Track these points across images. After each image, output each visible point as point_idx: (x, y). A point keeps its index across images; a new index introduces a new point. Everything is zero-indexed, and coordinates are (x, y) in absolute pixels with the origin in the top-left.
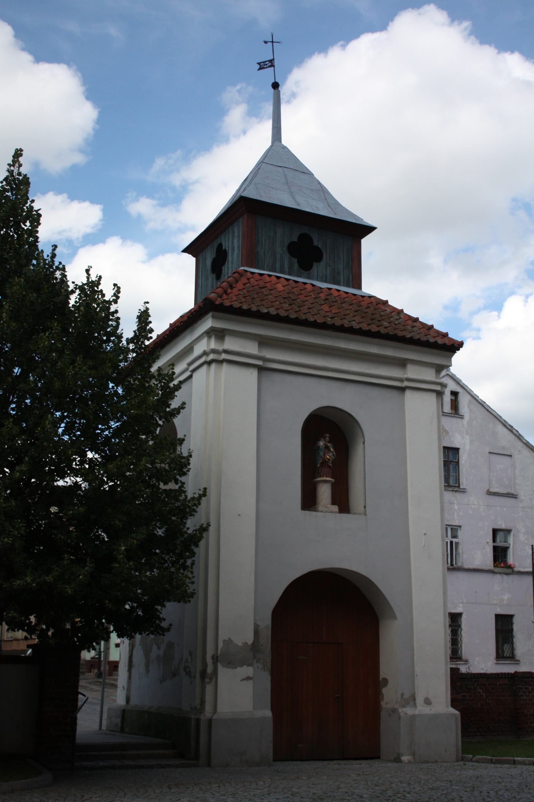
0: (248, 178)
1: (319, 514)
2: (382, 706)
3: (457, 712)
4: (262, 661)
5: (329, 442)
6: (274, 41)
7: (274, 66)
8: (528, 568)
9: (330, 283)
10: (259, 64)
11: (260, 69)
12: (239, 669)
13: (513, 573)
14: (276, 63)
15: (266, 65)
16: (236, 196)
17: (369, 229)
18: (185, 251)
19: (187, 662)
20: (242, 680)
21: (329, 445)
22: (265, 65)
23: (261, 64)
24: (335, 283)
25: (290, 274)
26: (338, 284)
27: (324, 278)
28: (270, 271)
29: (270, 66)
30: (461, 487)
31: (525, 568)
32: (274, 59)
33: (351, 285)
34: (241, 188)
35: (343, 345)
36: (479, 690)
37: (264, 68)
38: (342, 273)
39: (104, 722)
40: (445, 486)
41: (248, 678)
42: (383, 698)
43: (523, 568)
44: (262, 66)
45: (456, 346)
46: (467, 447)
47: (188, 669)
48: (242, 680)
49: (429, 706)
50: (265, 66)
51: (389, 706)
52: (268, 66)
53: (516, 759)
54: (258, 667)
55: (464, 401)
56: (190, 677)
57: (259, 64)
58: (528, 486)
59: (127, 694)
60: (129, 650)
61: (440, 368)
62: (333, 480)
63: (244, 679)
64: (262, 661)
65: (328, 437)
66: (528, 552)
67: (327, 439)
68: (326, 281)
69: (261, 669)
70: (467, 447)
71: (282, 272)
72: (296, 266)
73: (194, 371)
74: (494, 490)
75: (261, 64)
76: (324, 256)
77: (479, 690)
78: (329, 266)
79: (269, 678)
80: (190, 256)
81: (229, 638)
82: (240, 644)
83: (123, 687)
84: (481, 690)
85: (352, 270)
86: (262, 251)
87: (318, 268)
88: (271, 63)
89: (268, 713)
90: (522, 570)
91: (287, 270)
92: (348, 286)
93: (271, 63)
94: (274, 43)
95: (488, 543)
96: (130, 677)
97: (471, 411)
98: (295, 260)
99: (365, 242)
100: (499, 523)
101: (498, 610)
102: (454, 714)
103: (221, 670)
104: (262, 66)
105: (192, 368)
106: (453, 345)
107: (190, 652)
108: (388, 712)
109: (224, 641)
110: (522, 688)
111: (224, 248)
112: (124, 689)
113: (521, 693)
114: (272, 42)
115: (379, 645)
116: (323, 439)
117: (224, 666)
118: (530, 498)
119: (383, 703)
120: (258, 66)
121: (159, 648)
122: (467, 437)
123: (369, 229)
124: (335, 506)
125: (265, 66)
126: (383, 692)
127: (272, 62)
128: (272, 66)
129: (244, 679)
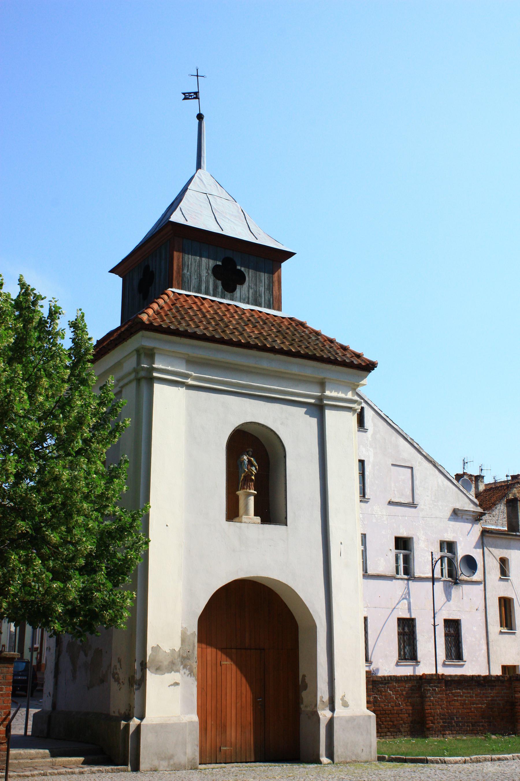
0: (174, 204)
1: (243, 525)
2: (301, 709)
3: (372, 714)
4: (189, 667)
5: (252, 457)
6: (199, 75)
7: (199, 99)
8: (428, 573)
9: (252, 304)
10: (184, 94)
11: (185, 99)
12: (167, 675)
13: (398, 576)
14: (201, 95)
15: (191, 96)
16: (162, 220)
17: (289, 255)
18: (111, 271)
19: (116, 669)
20: (169, 686)
21: (252, 459)
22: (190, 96)
23: (186, 95)
24: (256, 305)
25: (214, 295)
26: (260, 305)
27: (247, 300)
28: (196, 292)
29: (194, 98)
30: (366, 497)
31: (425, 574)
32: (198, 92)
33: (272, 307)
34: (167, 212)
35: (282, 368)
36: (389, 692)
37: (188, 99)
38: (263, 295)
39: (30, 727)
40: (360, 497)
41: (176, 684)
42: (302, 700)
43: (423, 574)
44: (187, 96)
45: (370, 366)
46: (371, 459)
47: (116, 676)
48: (169, 686)
49: (346, 708)
50: (190, 97)
51: (308, 709)
52: (193, 97)
53: (429, 758)
54: (185, 673)
55: (369, 414)
56: (119, 683)
57: (184, 94)
58: (428, 496)
59: (53, 700)
60: (56, 657)
61: (354, 388)
62: (256, 492)
63: (171, 685)
64: (189, 667)
65: (251, 451)
66: (428, 559)
67: (251, 453)
68: (248, 303)
69: (188, 675)
70: (371, 459)
71: (207, 293)
72: (220, 288)
73: (122, 387)
74: (394, 500)
75: (186, 95)
76: (247, 279)
77: (389, 692)
78: (251, 289)
79: (196, 683)
80: (118, 276)
81: (158, 645)
82: (168, 651)
83: (49, 693)
84: (391, 692)
85: (273, 292)
86: (188, 273)
87: (242, 290)
88: (196, 95)
89: (195, 718)
90: (423, 576)
91: (211, 292)
92: (269, 307)
93: (196, 95)
94: (199, 77)
95: (391, 550)
96: (56, 684)
97: (375, 425)
98: (219, 283)
99: (285, 265)
100: (401, 531)
101: (400, 613)
102: (370, 716)
103: (150, 676)
104: (187, 96)
105: (121, 384)
106: (368, 365)
107: (119, 658)
108: (307, 714)
109: (152, 648)
110: (430, 690)
111: (151, 269)
112: (50, 695)
113: (429, 695)
114: (197, 76)
115: (298, 650)
116: (246, 453)
117: (152, 672)
118: (430, 508)
119: (302, 706)
120: (183, 96)
121: (86, 655)
122: (371, 449)
123: (289, 255)
124: (257, 517)
125: (190, 97)
126: (303, 696)
127: (196, 93)
128: (197, 98)
129: (171, 685)
